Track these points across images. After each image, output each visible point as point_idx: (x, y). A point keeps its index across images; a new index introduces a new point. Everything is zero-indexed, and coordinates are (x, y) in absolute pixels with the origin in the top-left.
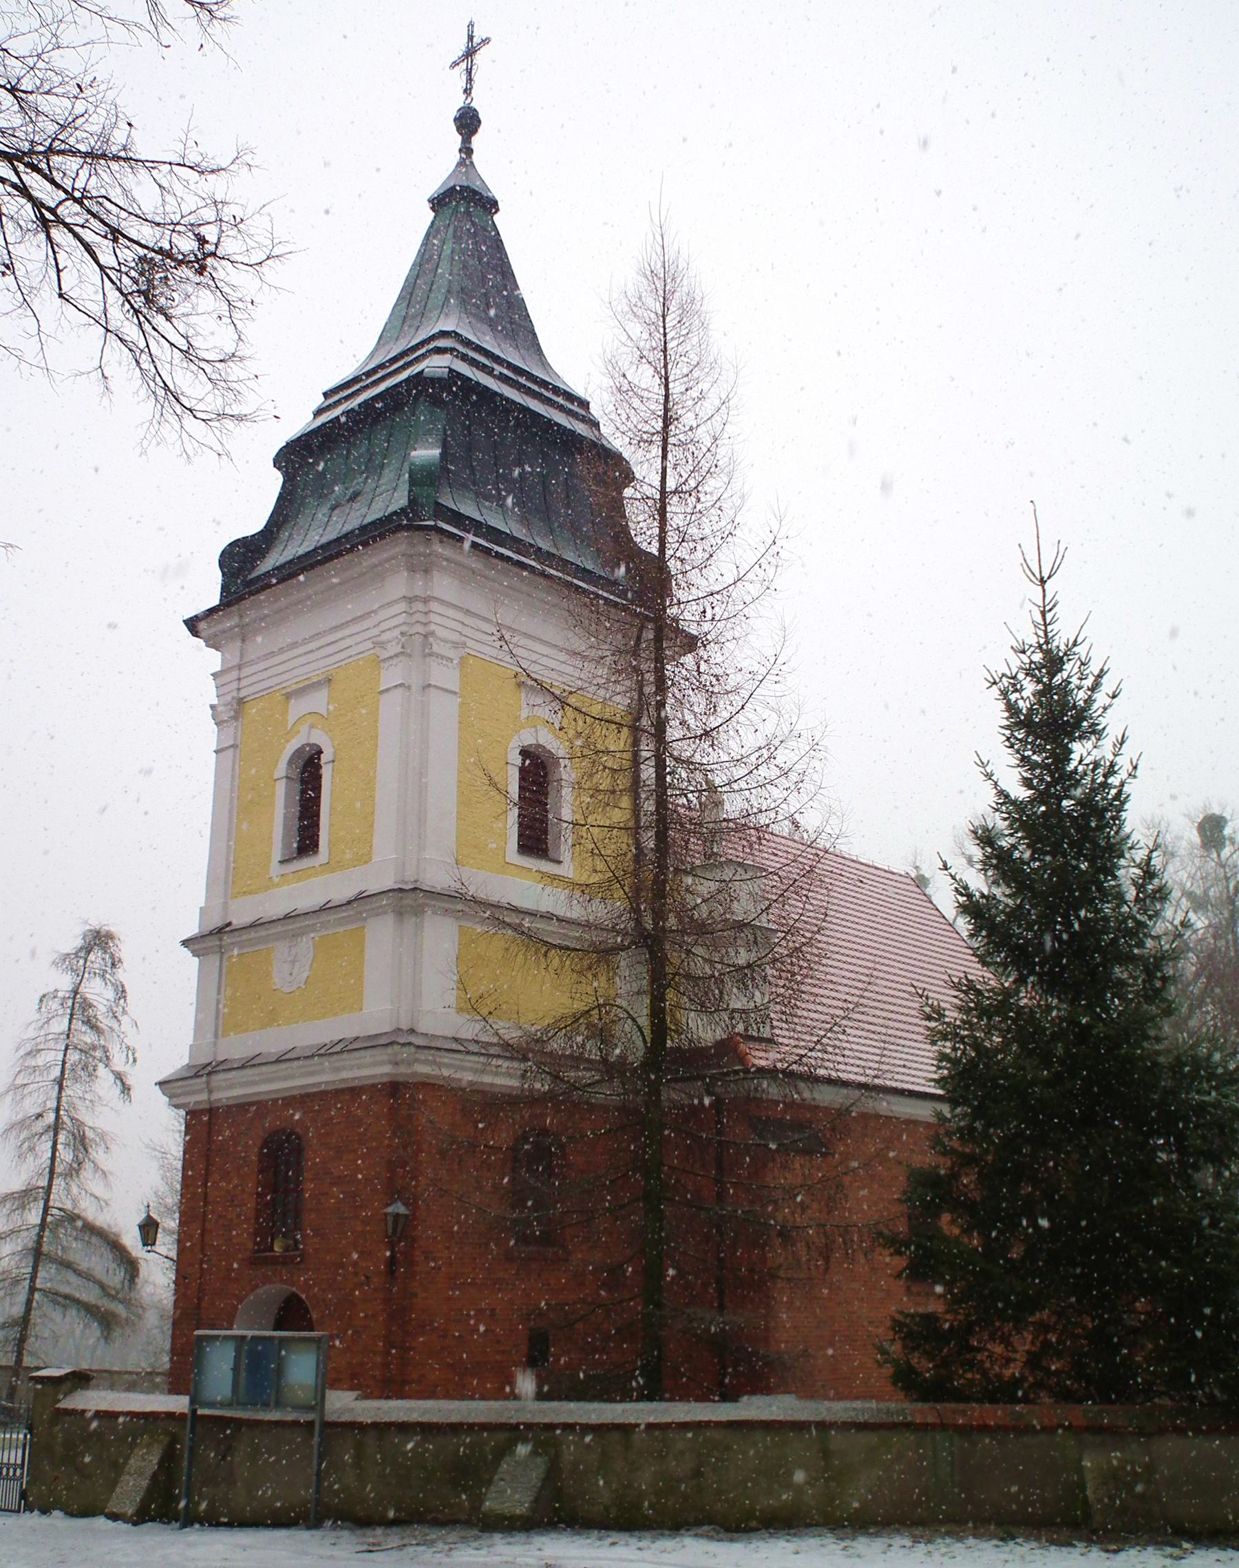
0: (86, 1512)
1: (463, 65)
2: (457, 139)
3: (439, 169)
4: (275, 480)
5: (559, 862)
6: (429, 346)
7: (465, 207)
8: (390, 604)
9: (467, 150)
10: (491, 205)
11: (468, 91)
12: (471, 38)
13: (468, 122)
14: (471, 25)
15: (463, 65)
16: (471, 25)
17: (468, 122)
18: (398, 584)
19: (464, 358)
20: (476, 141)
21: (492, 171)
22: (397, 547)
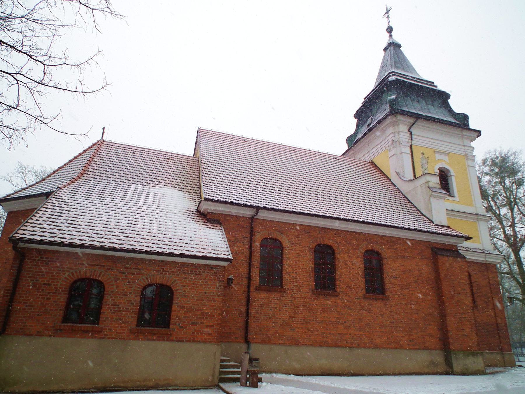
0: (161, 285)
1: (386, 16)
2: (388, 35)
3: (385, 40)
4: (355, 121)
5: (454, 197)
6: (388, 76)
7: (393, 47)
8: (389, 135)
9: (391, 36)
10: (399, 46)
11: (389, 22)
12: (387, 8)
13: (390, 30)
14: (386, 5)
15: (386, 16)
16: (386, 5)
17: (390, 30)
18: (390, 130)
19: (398, 76)
20: (392, 33)
21: (397, 37)
22: (390, 119)
